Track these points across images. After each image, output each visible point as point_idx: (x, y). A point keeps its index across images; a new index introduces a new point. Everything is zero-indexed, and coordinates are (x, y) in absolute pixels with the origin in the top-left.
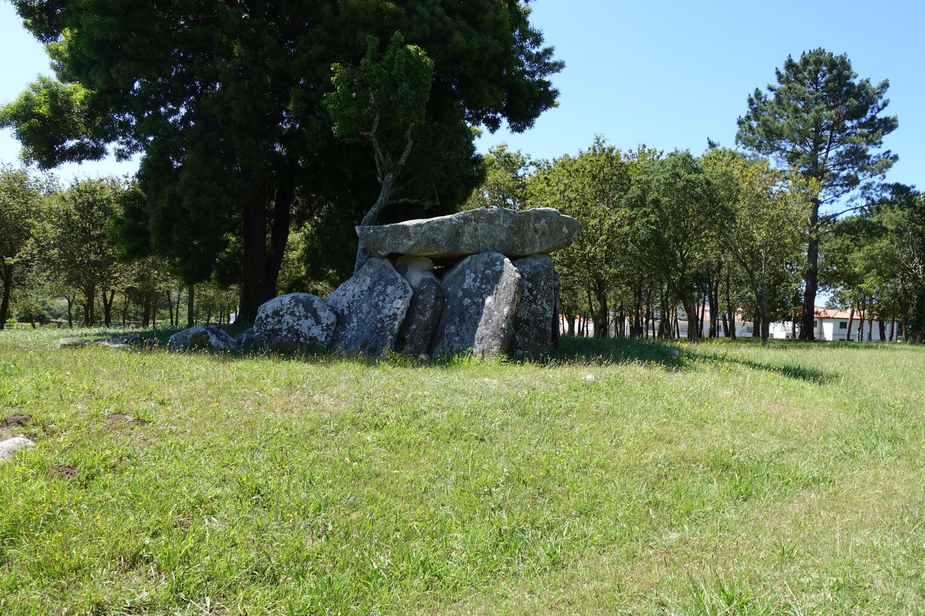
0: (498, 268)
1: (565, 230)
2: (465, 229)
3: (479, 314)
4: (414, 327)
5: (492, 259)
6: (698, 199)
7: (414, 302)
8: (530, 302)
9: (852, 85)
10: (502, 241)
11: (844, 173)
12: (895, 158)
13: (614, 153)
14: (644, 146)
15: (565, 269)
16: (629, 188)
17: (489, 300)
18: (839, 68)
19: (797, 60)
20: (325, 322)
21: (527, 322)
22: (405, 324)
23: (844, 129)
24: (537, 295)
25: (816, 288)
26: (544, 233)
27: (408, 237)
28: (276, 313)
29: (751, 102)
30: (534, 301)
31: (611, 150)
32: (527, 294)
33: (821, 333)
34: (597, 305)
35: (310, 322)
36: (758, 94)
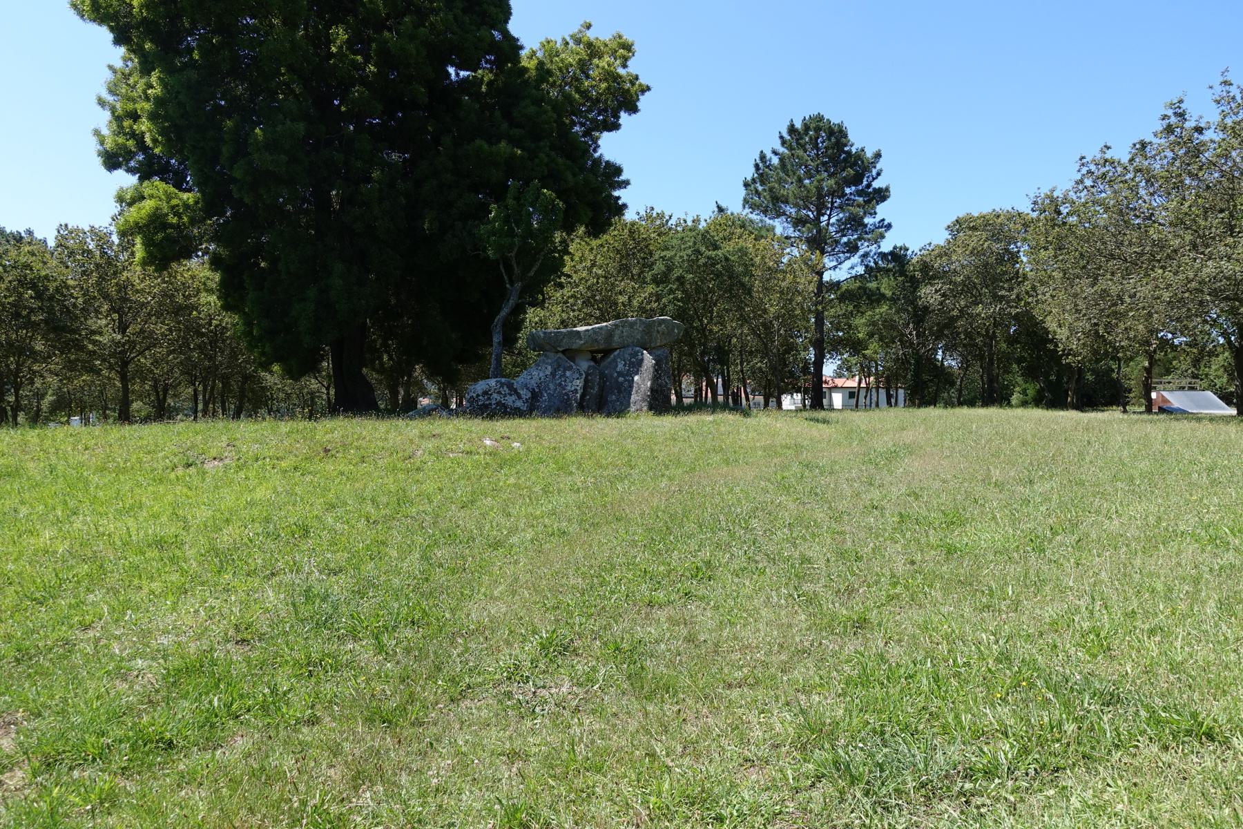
3: (631, 387)
6: (718, 275)
7: (586, 381)
9: (849, 153)
11: (845, 239)
12: (889, 226)
14: (652, 209)
17: (636, 378)
18: (838, 135)
19: (798, 125)
23: (844, 195)
25: (824, 356)
27: (580, 338)
28: (485, 393)
29: (757, 166)
33: (831, 404)
35: (514, 398)
36: (763, 157)
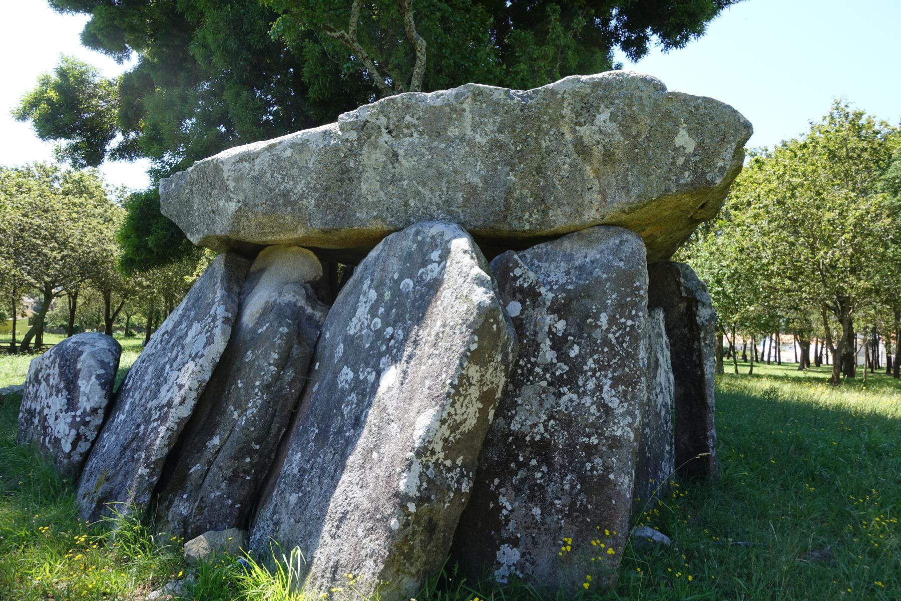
0: (433, 269)
1: (684, 140)
2: (364, 159)
4: (216, 441)
5: (421, 244)
8: (557, 382)
10: (474, 188)
13: (863, 121)
15: (788, 282)
16: (889, 166)
17: (390, 377)
20: (85, 404)
21: (543, 449)
22: (189, 436)
24: (582, 358)
26: (608, 157)
30: (570, 381)
31: (859, 115)
32: (548, 355)
34: (837, 330)
